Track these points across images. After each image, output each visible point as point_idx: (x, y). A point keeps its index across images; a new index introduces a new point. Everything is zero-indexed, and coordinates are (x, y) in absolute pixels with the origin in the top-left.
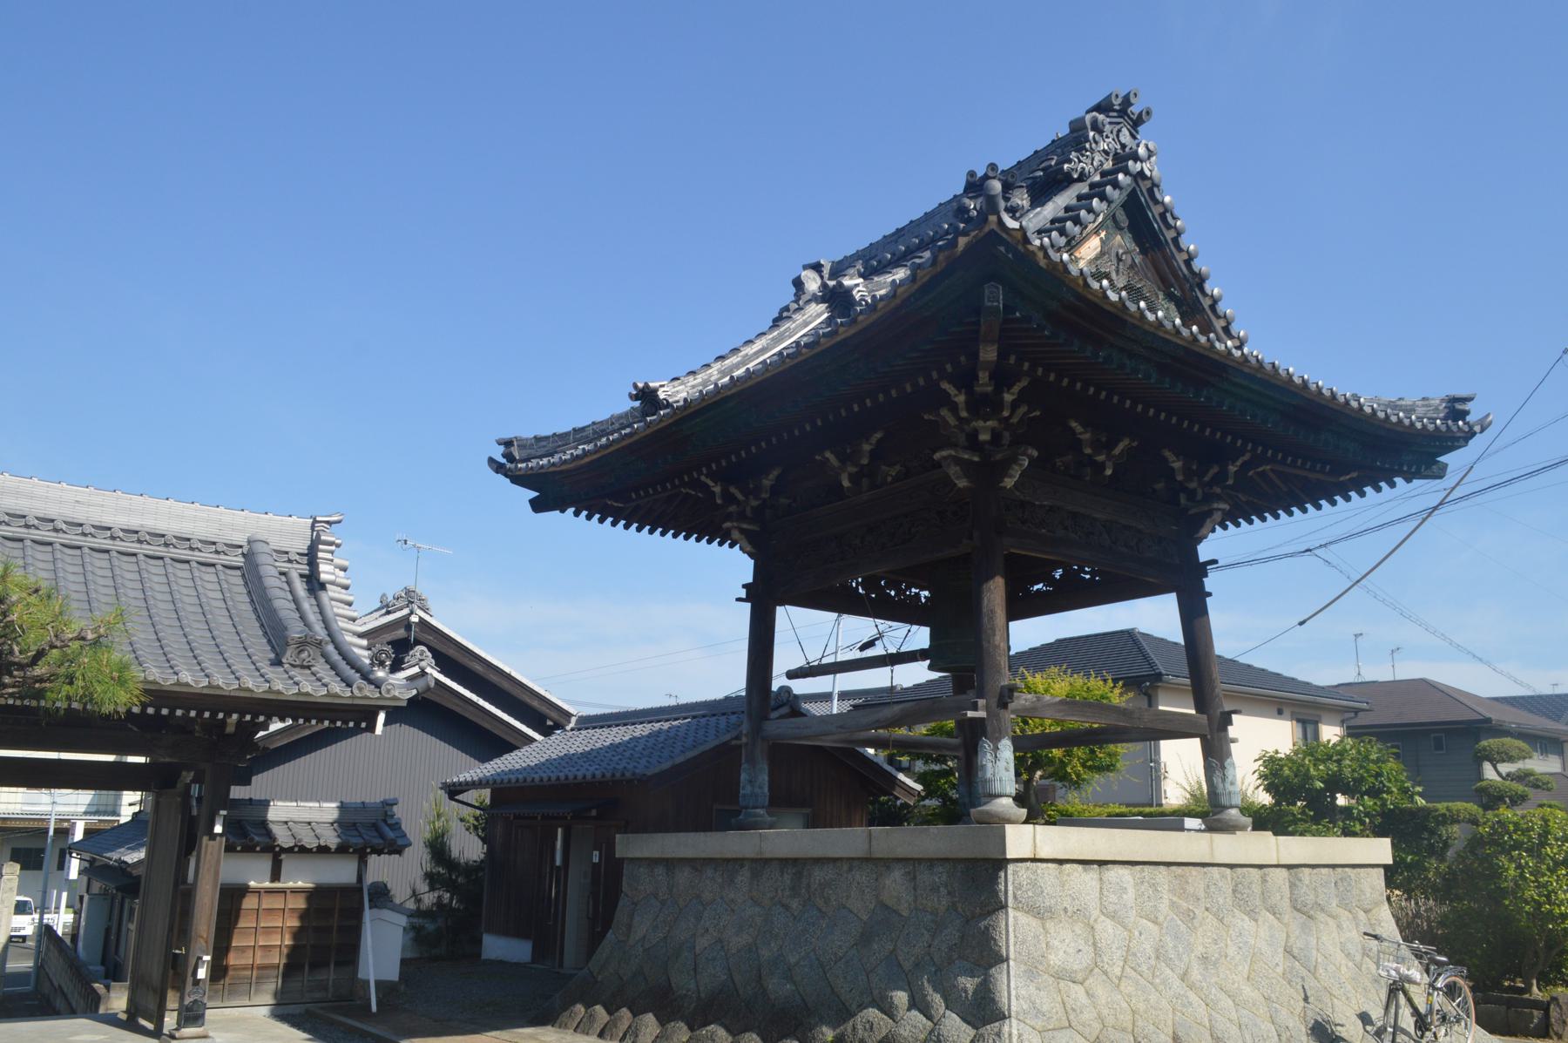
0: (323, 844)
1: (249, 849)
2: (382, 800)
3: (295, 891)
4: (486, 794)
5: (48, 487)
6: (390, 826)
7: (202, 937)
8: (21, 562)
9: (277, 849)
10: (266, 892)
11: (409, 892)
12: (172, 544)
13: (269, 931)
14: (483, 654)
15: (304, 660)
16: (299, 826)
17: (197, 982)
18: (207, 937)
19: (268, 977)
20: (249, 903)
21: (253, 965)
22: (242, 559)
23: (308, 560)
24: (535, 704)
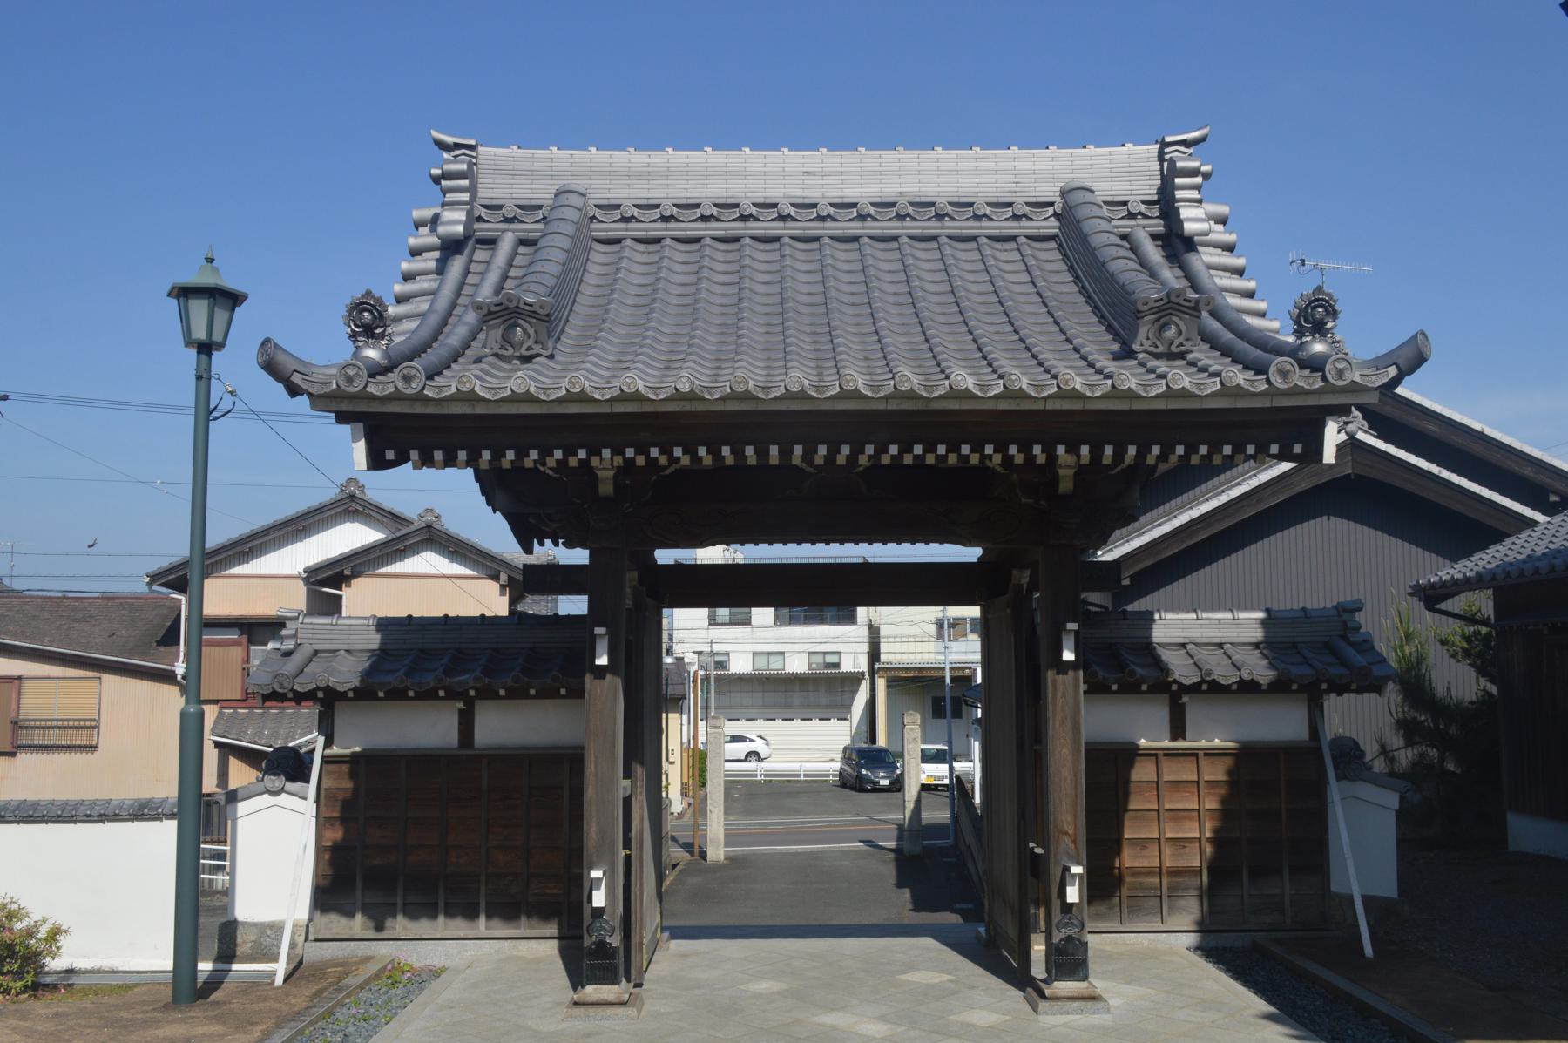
0: (1246, 677)
1: (1130, 688)
2: (1335, 604)
3: (1211, 753)
4: (1483, 602)
5: (765, 157)
6: (1353, 644)
7: (1067, 833)
8: (831, 355)
9: (1174, 687)
10: (1165, 755)
11: (1376, 747)
12: (947, 215)
13: (1178, 815)
14: (1437, 408)
15: (1172, 342)
16: (1204, 651)
17: (1067, 908)
18: (1075, 834)
19: (1187, 888)
20: (1142, 772)
21: (1160, 868)
22: (1054, 223)
23: (1160, 209)
24: (1528, 472)
